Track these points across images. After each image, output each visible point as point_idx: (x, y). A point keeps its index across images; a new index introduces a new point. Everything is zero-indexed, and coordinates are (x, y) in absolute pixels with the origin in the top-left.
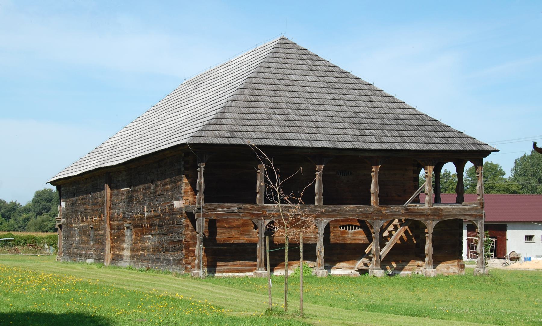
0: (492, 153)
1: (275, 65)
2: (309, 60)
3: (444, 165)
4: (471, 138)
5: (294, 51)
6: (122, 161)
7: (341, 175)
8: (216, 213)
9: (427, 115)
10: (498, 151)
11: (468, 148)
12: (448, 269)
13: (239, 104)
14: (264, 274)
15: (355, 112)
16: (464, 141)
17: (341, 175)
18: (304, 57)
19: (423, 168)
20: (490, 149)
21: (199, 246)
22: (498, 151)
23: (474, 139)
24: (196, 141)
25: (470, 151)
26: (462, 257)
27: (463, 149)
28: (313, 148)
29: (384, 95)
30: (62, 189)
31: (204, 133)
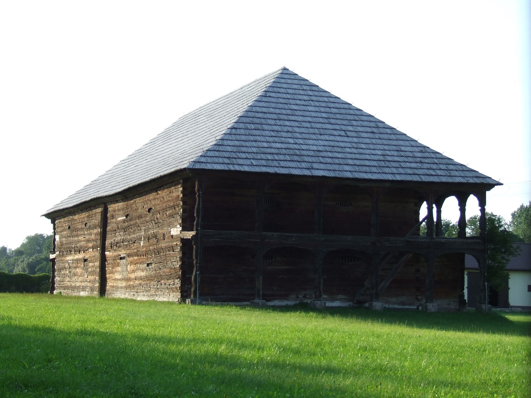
0: (495, 186)
1: (329, 149)
2: (310, 90)
3: (446, 199)
4: (450, 159)
5: (296, 82)
6: (120, 190)
7: (340, 205)
8: (214, 239)
9: (429, 147)
10: (502, 184)
11: (471, 181)
12: (449, 304)
13: (238, 131)
14: (261, 303)
15: (348, 137)
16: (468, 174)
17: (340, 205)
18: (305, 88)
19: (425, 203)
20: (494, 183)
21: (196, 272)
22: (502, 184)
23: (296, 76)
24: (198, 166)
25: (473, 183)
26: (464, 293)
27: (466, 182)
28: (313, 177)
29: (385, 127)
30: (57, 221)
31: (203, 159)
